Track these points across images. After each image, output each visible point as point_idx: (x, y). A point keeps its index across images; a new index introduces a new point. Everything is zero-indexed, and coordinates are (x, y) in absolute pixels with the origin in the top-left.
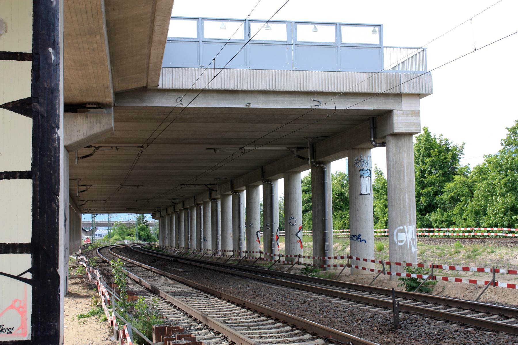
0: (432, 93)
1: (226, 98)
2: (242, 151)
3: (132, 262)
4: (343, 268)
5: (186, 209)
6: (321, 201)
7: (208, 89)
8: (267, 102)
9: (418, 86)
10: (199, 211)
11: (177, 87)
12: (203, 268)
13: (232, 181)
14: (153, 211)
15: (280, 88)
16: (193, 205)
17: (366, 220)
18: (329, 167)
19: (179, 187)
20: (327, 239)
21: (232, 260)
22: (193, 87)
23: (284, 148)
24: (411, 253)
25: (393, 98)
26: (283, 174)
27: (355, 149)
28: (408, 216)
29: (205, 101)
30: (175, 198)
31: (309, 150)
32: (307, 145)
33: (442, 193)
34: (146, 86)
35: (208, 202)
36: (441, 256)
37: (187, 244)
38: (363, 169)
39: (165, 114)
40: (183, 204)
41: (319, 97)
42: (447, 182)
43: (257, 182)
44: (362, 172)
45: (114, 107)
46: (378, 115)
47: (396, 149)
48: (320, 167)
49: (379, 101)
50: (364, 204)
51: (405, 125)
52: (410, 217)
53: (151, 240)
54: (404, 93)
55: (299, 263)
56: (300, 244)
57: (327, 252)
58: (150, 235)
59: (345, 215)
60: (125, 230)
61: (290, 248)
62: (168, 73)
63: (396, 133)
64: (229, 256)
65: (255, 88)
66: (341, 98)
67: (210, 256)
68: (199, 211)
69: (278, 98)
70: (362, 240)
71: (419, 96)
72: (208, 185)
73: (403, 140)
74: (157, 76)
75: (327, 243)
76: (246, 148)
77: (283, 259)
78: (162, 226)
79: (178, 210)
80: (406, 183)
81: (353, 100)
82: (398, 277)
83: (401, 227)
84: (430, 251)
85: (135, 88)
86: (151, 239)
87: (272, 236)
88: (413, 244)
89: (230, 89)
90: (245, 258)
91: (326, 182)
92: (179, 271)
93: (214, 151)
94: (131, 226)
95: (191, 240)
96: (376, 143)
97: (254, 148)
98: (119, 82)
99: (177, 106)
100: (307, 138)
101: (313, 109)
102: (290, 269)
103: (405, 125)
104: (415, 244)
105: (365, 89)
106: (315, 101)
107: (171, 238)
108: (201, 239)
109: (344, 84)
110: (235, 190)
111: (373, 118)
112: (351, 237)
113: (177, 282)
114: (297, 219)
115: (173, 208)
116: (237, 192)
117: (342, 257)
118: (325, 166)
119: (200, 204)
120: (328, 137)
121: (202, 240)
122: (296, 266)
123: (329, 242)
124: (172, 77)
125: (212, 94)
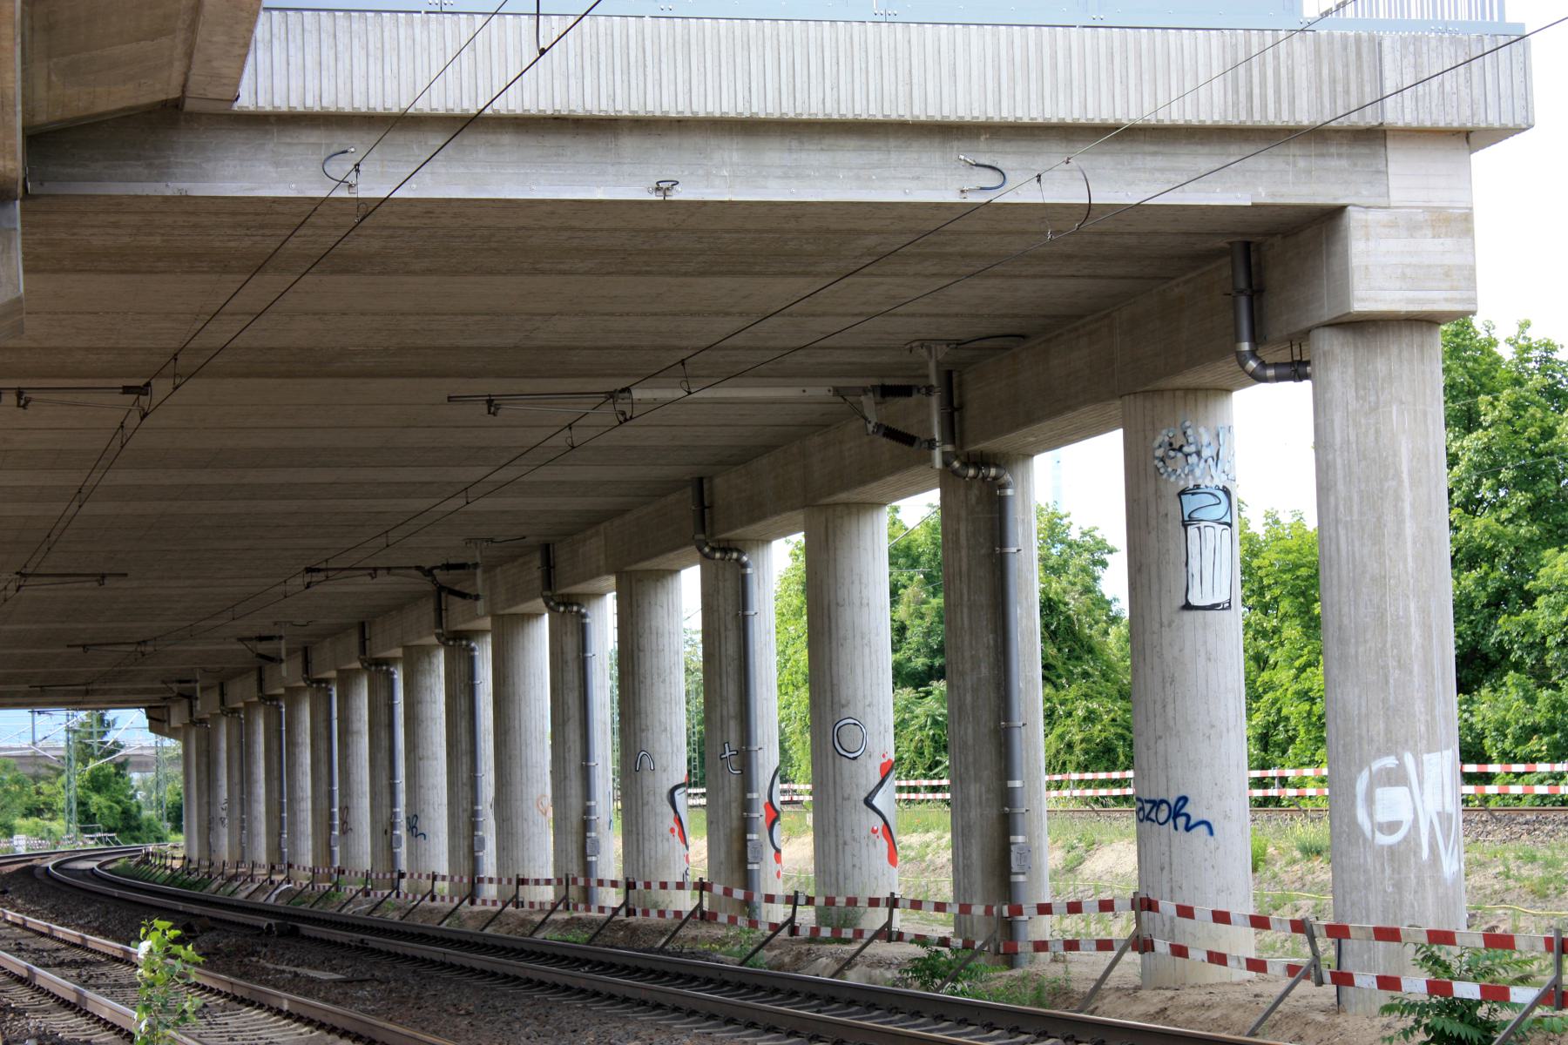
0: (1530, 126)
1: (557, 155)
2: (618, 407)
3: (78, 941)
4: (1112, 954)
5: (320, 685)
6: (988, 639)
7: (427, 110)
8: (754, 171)
9: (1464, 91)
10: (382, 696)
11: (325, 104)
12: (432, 962)
13: (547, 550)
14: (157, 697)
15: (813, 104)
16: (357, 665)
17: (1213, 726)
18: (1026, 478)
19: (299, 582)
20: (1019, 818)
21: (555, 921)
22: (419, 105)
23: (820, 391)
24: (1438, 880)
25: (1344, 150)
26: (799, 516)
27: (1154, 391)
28: (1419, 707)
29: (462, 170)
30: (266, 633)
31: (935, 402)
32: (927, 376)
33: (1529, 599)
34: (179, 98)
35: (427, 652)
36: (1546, 896)
37: (324, 849)
38: (1197, 487)
39: (267, 232)
40: (306, 663)
41: (998, 146)
42: (1551, 545)
43: (671, 555)
44: (1190, 503)
45: (22, 200)
46: (1270, 234)
47: (1362, 393)
48: (984, 478)
49: (1279, 164)
50: (1202, 653)
51: (1404, 277)
52: (1431, 710)
53: (137, 834)
54: (1400, 124)
55: (891, 933)
56: (883, 844)
57: (1021, 878)
58: (134, 809)
59: (1069, 707)
60: (14, 788)
61: (837, 864)
62: (284, 36)
63: (1359, 314)
64: (541, 904)
65: (695, 108)
66: (1104, 154)
67: (448, 905)
68: (382, 696)
69: (804, 155)
70: (1192, 822)
71: (1467, 138)
72: (435, 571)
73: (1394, 350)
74: (237, 51)
75: (1020, 839)
76: (637, 394)
77: (807, 917)
78: (202, 765)
79: (282, 691)
80: (1409, 552)
81: (1159, 162)
82: (1384, 997)
83: (1390, 762)
84: (1492, 871)
85: (123, 109)
86: (139, 828)
87: (747, 806)
88: (1447, 837)
89: (580, 112)
90: (623, 912)
91: (1014, 550)
92: (321, 982)
93: (486, 407)
94: (43, 771)
95: (346, 829)
96: (1263, 365)
97: (681, 393)
98: (54, 78)
99: (334, 195)
100: (924, 343)
101: (978, 206)
102: (849, 963)
103: (1404, 277)
104: (1456, 841)
105: (1216, 110)
106: (977, 165)
107: (244, 825)
108: (393, 825)
109: (1117, 85)
110: (559, 592)
111: (1247, 245)
112: (1142, 809)
113: (329, 1032)
114: (871, 726)
115: (252, 681)
116: (572, 604)
117: (1106, 906)
118: (1008, 477)
119: (389, 662)
120: (1023, 336)
121: (402, 831)
122: (881, 949)
123: (1029, 835)
124: (300, 55)
125: (492, 138)
